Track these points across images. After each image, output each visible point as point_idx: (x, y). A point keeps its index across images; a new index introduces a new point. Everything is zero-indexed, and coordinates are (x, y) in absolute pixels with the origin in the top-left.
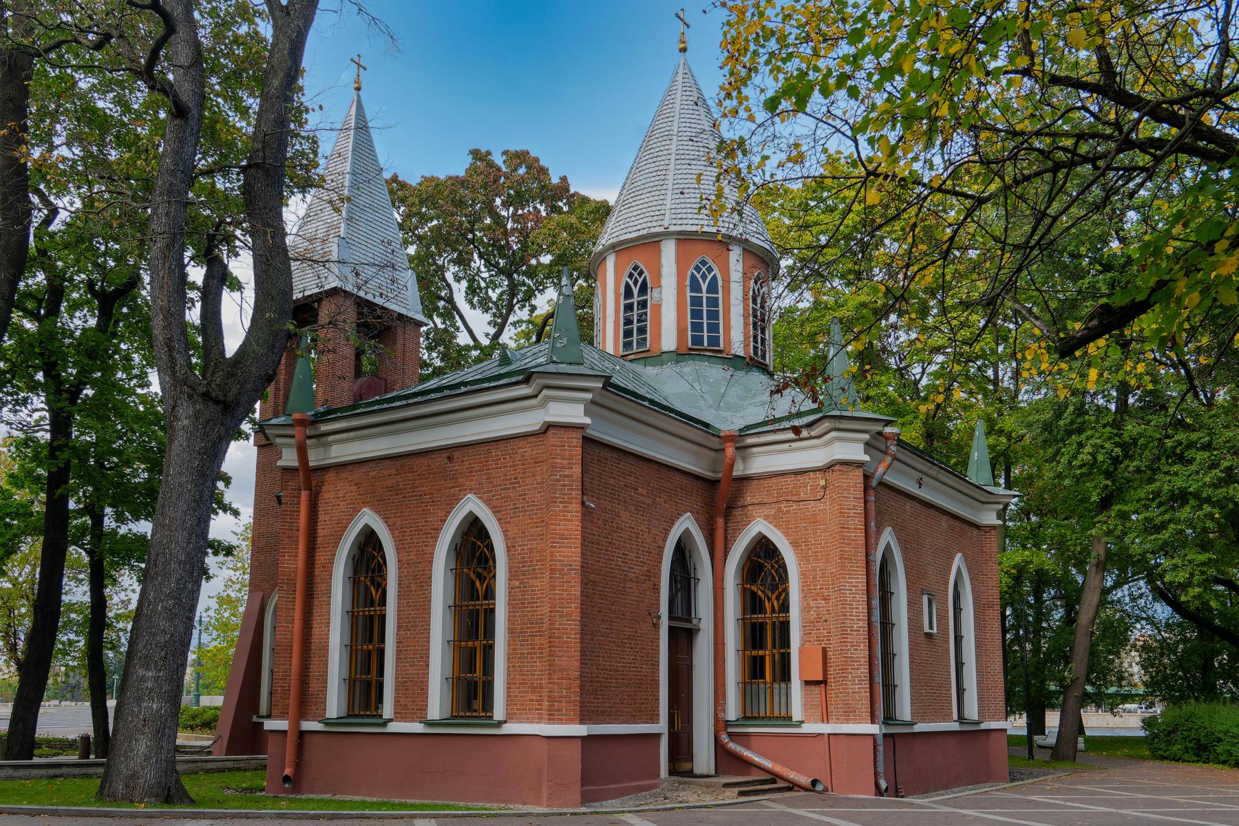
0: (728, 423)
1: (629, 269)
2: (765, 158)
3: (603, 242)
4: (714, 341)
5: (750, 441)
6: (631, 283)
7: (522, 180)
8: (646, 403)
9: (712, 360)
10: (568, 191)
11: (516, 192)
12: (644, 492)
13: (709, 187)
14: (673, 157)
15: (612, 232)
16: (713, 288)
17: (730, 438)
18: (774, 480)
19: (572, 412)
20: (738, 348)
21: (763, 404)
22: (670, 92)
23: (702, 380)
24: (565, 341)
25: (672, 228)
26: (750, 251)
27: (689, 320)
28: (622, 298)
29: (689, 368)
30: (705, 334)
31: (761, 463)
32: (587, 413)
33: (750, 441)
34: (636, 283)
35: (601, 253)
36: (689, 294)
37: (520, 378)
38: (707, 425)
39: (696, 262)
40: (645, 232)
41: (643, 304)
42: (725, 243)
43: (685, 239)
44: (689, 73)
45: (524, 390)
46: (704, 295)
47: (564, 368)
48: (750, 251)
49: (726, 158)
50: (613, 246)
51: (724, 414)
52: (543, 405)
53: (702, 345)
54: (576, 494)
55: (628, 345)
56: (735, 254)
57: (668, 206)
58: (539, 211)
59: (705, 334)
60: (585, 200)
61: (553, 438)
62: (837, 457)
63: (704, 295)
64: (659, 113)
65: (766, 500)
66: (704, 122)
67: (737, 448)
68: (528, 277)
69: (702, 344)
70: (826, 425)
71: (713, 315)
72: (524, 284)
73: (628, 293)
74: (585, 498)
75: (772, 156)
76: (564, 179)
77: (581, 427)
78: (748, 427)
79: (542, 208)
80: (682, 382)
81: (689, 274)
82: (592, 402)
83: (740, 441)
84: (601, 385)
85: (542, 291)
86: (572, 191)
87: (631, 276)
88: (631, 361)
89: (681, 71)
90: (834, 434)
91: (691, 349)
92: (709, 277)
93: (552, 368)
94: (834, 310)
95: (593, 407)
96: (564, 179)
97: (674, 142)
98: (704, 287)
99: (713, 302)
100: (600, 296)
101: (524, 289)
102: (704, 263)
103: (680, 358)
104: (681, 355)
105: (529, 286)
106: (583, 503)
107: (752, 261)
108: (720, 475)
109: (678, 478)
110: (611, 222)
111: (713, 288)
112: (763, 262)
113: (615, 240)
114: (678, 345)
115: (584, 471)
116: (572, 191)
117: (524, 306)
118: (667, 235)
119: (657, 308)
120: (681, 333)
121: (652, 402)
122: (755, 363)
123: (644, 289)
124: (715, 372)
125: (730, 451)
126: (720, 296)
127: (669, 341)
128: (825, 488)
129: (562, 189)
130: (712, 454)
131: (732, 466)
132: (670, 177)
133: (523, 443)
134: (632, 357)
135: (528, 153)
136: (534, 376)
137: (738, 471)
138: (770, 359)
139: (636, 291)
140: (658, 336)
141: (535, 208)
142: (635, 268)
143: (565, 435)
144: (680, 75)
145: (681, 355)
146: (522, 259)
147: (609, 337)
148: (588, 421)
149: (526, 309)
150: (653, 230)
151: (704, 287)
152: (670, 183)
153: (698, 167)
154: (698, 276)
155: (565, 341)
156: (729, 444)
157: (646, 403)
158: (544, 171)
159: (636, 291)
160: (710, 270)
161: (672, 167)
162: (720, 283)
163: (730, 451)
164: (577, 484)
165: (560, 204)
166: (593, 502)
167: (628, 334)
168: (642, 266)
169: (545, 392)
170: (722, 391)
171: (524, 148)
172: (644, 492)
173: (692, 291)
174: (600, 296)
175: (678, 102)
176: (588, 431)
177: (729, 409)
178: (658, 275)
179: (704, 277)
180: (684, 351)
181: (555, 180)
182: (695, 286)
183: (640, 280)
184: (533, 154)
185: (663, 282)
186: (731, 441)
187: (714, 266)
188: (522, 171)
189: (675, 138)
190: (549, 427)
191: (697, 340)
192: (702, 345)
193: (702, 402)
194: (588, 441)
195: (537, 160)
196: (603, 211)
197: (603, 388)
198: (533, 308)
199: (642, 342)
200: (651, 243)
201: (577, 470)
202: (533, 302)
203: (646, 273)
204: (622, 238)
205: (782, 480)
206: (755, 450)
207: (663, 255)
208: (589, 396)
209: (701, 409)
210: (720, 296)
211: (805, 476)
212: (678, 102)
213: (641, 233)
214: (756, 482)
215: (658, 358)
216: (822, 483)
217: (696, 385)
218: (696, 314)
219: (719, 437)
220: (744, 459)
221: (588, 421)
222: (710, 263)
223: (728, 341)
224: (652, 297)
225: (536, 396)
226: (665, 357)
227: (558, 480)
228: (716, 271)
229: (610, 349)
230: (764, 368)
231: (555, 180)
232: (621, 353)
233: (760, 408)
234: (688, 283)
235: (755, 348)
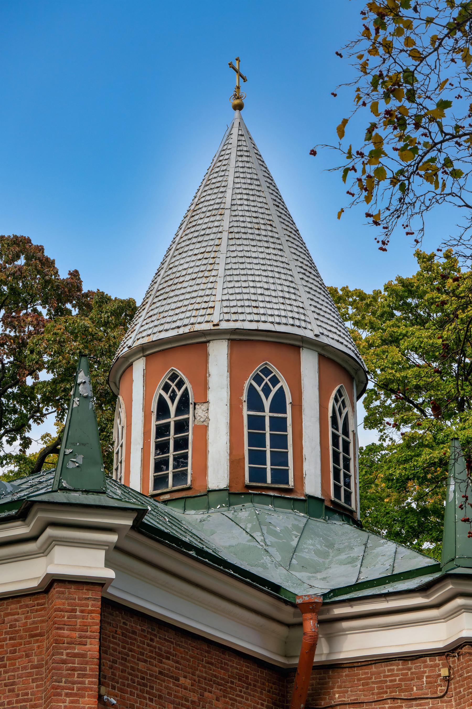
0: (307, 585)
1: (164, 379)
2: (444, 105)
3: (130, 343)
4: (280, 476)
5: (338, 611)
6: (166, 397)
7: (19, 274)
8: (192, 553)
9: (278, 502)
10: (80, 289)
11: (12, 289)
12: (187, 682)
13: (356, 139)
14: (225, 236)
15: (137, 335)
16: (279, 404)
17: (310, 607)
18: (374, 669)
19: (87, 562)
20: (313, 486)
21: (352, 561)
22: (221, 158)
23: (265, 529)
24: (80, 459)
25: (224, 326)
26: (329, 358)
27: (246, 448)
28: (154, 417)
29: (246, 513)
30: (269, 467)
31: (357, 643)
32: (108, 563)
33: (338, 611)
34: (172, 398)
35: (126, 358)
36: (246, 412)
37: (13, 512)
38: (276, 588)
39: (256, 370)
40: (186, 330)
41: (182, 426)
42: (291, 345)
43: (240, 340)
44: (245, 134)
45: (18, 530)
46: (267, 414)
47: (76, 497)
48: (329, 358)
49: (387, 96)
50: (143, 349)
51: (298, 575)
52: (45, 551)
53: (263, 481)
54: (91, 682)
55: (160, 481)
56: (309, 364)
57: (219, 297)
58: (40, 314)
59: (269, 467)
60: (103, 299)
61: (58, 598)
62: (465, 634)
63: (267, 414)
64: (207, 182)
65: (362, 698)
66: (266, 194)
67: (320, 622)
68: (21, 403)
69: (265, 482)
70: (449, 587)
71: (280, 441)
72: (15, 411)
73: (163, 410)
74: (103, 689)
75: (455, 103)
76: (75, 274)
77: (99, 584)
78: (336, 592)
79: (44, 312)
80: (237, 531)
81: (246, 386)
82: (117, 548)
83: (326, 611)
84: (129, 523)
85: (39, 420)
86: (85, 290)
87: (166, 388)
88: (166, 502)
89: (235, 131)
90: (459, 601)
91: (248, 487)
92: (274, 390)
93: (60, 497)
94: (432, 447)
95: (117, 554)
96: (75, 274)
97: (227, 218)
98: (267, 404)
99: (279, 424)
100: (123, 415)
101: (14, 417)
102: (266, 371)
103: (233, 499)
104: (234, 495)
105: (21, 413)
106: (100, 697)
107: (331, 371)
108: (296, 661)
109: (236, 666)
110: (140, 320)
111: (279, 404)
112: (343, 371)
113: (146, 340)
114: (231, 480)
115: (102, 649)
116: (85, 290)
117: (14, 439)
118: (216, 334)
119: (203, 430)
120: (235, 464)
121: (200, 552)
122: (335, 508)
123: (184, 406)
124: (285, 520)
125: (310, 624)
126: (289, 415)
127: (218, 476)
128: (448, 679)
129: (71, 289)
130: (283, 630)
131: (313, 647)
132: (222, 261)
133: (13, 607)
134: (167, 497)
135: (29, 241)
136: (35, 508)
137: (322, 654)
138: (355, 505)
139: (173, 409)
140: (203, 469)
141: (35, 310)
142: (173, 377)
143: (76, 594)
144: (235, 137)
145: (234, 495)
146: (13, 377)
147: (135, 471)
148: (110, 574)
149: (18, 442)
150: (197, 328)
151: (267, 404)
152: (221, 267)
153: (346, 105)
154: (259, 389)
155: (80, 459)
156: (308, 616)
157: (192, 553)
158: (49, 263)
159: (173, 409)
160: (275, 381)
161: (223, 248)
162: (289, 399)
163: (310, 624)
164: (92, 668)
165: (69, 306)
166: (115, 696)
167: (161, 465)
168: (182, 375)
169: (50, 531)
170: (294, 543)
171: (20, 233)
172: (187, 682)
173: (249, 408)
174: (123, 415)
175: (232, 169)
176: (110, 590)
177: (304, 568)
178: (203, 386)
179: (267, 391)
180: (238, 489)
181: (64, 275)
182: (255, 402)
183: (179, 394)
184: (35, 242)
185: (211, 396)
186: (312, 611)
187: (280, 377)
188: (21, 261)
189: (227, 212)
190: (53, 582)
191: (257, 475)
192: (263, 481)
193: (266, 559)
194: (110, 606)
195: (41, 249)
196: (126, 312)
197: (133, 528)
198: (27, 443)
199: (180, 476)
200: (194, 344)
201: (92, 647)
202: (27, 435)
203: (187, 384)
204: (154, 338)
205: (385, 668)
206: (345, 624)
207: (211, 359)
208: (113, 538)
209: (265, 567)
210: (289, 415)
211: (419, 663)
212: (232, 169)
213: (181, 331)
214: (346, 672)
215: (204, 498)
216: (444, 672)
217: (257, 535)
218: (256, 440)
219: (294, 605)
220: (330, 638)
221: (110, 574)
222: (276, 372)
223: (300, 477)
224: (196, 415)
225: (34, 539)
226: (212, 497)
227: (64, 662)
228: (283, 383)
229: (135, 483)
230: (347, 516)
231: (64, 275)
232: (151, 490)
233: (348, 568)
234: (245, 397)
235: (337, 488)
